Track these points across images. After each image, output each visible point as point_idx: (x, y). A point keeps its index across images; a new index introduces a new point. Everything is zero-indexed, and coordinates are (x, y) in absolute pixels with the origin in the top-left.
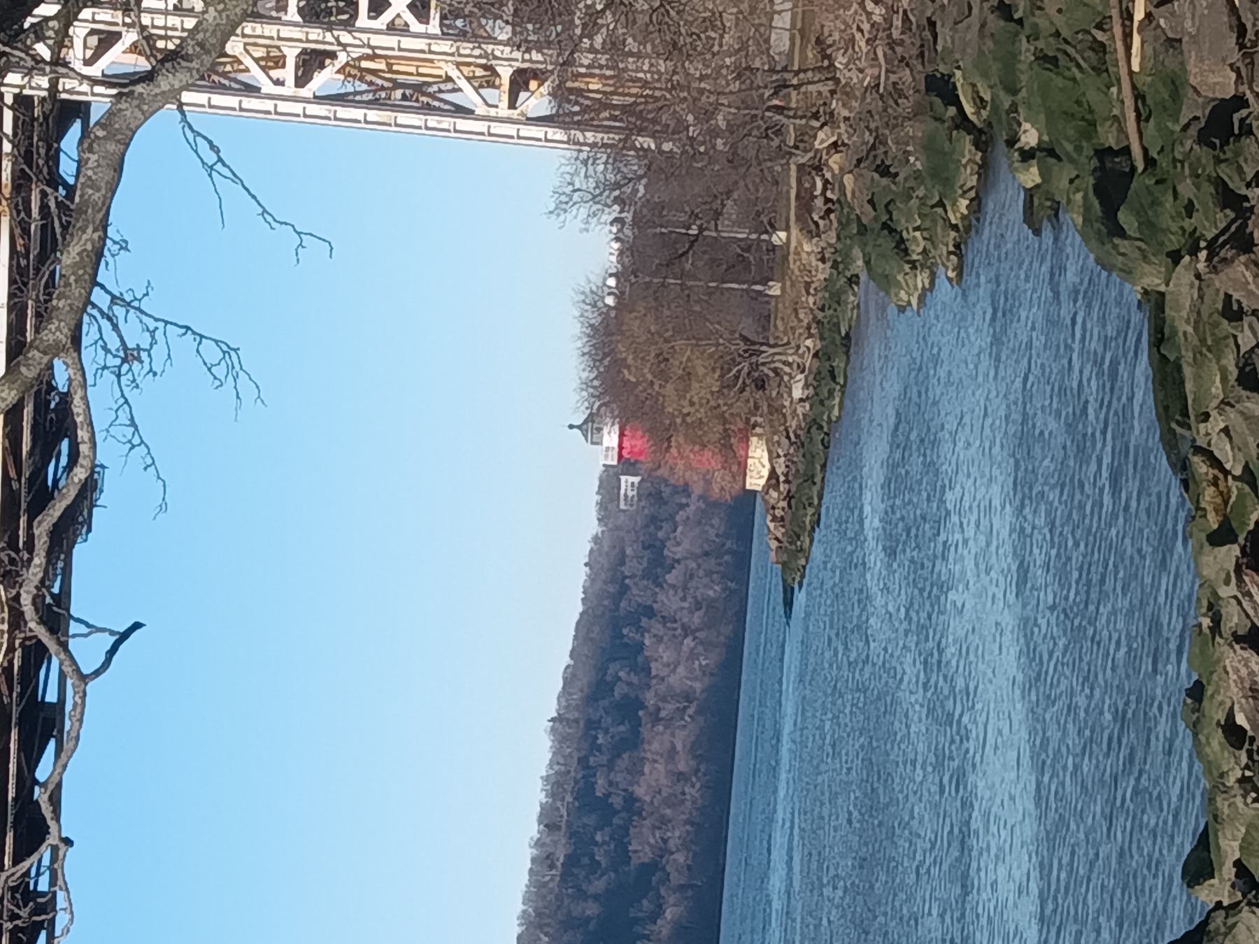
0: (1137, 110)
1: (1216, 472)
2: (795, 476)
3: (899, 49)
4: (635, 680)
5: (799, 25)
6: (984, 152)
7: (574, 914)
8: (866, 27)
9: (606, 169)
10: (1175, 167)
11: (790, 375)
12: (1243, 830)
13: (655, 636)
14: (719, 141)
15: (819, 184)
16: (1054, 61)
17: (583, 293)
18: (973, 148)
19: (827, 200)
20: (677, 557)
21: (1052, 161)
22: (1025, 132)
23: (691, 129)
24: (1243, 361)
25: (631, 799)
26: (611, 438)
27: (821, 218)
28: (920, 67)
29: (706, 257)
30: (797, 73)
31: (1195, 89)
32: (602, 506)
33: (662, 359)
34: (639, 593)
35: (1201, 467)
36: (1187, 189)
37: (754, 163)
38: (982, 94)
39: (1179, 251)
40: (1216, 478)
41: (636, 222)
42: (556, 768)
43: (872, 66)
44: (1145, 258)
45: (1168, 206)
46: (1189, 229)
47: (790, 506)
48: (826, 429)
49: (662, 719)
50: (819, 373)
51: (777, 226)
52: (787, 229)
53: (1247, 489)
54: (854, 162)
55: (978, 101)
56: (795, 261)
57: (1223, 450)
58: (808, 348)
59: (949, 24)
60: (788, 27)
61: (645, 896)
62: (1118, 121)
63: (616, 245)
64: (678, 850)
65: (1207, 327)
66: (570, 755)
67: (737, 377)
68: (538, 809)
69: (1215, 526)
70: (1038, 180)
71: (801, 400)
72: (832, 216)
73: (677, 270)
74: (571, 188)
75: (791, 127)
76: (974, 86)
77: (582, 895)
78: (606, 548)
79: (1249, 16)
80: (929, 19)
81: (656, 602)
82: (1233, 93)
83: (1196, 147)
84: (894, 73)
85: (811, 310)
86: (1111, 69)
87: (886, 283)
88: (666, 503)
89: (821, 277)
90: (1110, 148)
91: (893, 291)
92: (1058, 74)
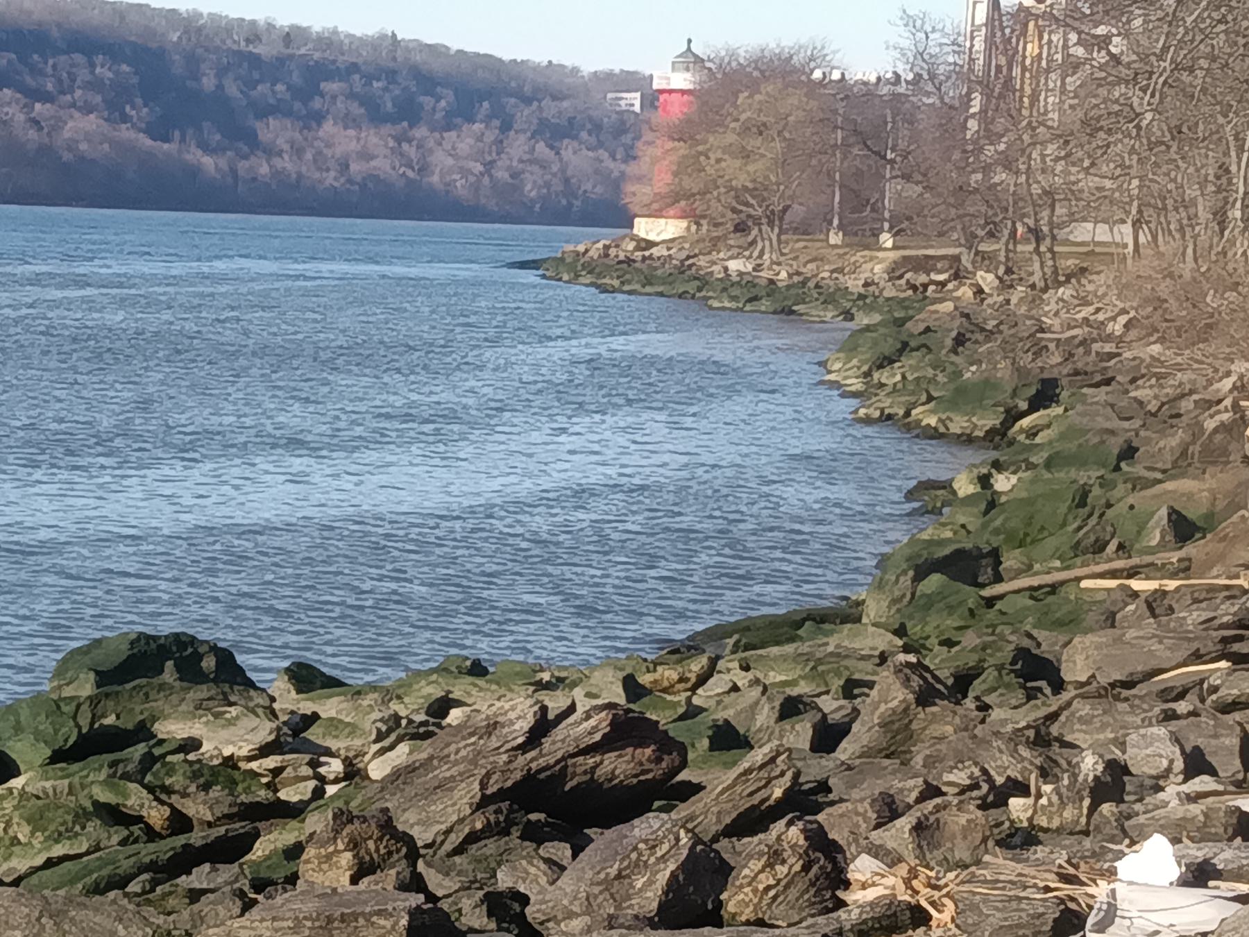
0: (1040, 587)
1: (693, 680)
2: (650, 266)
3: (1081, 350)
4: (439, 115)
5: (1098, 250)
6: (984, 438)
7: (203, 66)
8: (1101, 317)
9: (950, 64)
10: (987, 627)
11: (750, 257)
12: (348, 720)
13: (483, 134)
14: (979, 176)
15: (941, 277)
16: (1082, 503)
17: (823, 48)
18: (987, 428)
19: (925, 286)
20: (562, 152)
21: (983, 506)
22: (1008, 479)
23: (992, 148)
24: (808, 700)
25: (319, 118)
26: (682, 80)
27: (908, 281)
28: (1065, 372)
29: (865, 168)
30: (1051, 250)
31: (1070, 642)
32: (609, 75)
33: (762, 129)
34: (524, 115)
35: (697, 665)
36: (970, 639)
37: (961, 212)
38: (1041, 434)
39: (906, 635)
40: (687, 680)
41: (896, 96)
42: (347, 41)
43: (1062, 325)
44: (894, 601)
45: (948, 622)
46: (928, 643)
47: (620, 262)
48: (698, 295)
49: (400, 144)
50: (755, 286)
51: (898, 238)
52: (895, 248)
53: (681, 710)
54: (966, 311)
55: (1034, 431)
56: (863, 257)
57: (717, 685)
58: (778, 274)
59: (1110, 399)
60: (1096, 239)
61: (223, 136)
62: (1028, 569)
63: (873, 79)
64: (271, 167)
65: (836, 666)
66: (360, 55)
67: (747, 204)
68: (305, 25)
69: (640, 680)
70: (961, 494)
71: (726, 269)
72: (910, 292)
73: (852, 140)
74: (929, 29)
75: (996, 247)
76: (1048, 426)
77: (221, 72)
78: (567, 80)
79: (1144, 692)
80: (1113, 378)
81: (517, 132)
82: (1066, 678)
83: (1012, 647)
84: (1057, 347)
85: (816, 275)
86: (1078, 561)
87: (849, 348)
88: (615, 138)
89: (850, 284)
90: (1001, 563)
91: (841, 355)
92: (1070, 509)
